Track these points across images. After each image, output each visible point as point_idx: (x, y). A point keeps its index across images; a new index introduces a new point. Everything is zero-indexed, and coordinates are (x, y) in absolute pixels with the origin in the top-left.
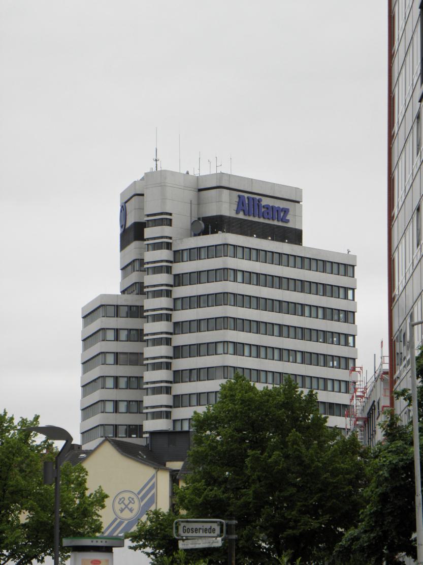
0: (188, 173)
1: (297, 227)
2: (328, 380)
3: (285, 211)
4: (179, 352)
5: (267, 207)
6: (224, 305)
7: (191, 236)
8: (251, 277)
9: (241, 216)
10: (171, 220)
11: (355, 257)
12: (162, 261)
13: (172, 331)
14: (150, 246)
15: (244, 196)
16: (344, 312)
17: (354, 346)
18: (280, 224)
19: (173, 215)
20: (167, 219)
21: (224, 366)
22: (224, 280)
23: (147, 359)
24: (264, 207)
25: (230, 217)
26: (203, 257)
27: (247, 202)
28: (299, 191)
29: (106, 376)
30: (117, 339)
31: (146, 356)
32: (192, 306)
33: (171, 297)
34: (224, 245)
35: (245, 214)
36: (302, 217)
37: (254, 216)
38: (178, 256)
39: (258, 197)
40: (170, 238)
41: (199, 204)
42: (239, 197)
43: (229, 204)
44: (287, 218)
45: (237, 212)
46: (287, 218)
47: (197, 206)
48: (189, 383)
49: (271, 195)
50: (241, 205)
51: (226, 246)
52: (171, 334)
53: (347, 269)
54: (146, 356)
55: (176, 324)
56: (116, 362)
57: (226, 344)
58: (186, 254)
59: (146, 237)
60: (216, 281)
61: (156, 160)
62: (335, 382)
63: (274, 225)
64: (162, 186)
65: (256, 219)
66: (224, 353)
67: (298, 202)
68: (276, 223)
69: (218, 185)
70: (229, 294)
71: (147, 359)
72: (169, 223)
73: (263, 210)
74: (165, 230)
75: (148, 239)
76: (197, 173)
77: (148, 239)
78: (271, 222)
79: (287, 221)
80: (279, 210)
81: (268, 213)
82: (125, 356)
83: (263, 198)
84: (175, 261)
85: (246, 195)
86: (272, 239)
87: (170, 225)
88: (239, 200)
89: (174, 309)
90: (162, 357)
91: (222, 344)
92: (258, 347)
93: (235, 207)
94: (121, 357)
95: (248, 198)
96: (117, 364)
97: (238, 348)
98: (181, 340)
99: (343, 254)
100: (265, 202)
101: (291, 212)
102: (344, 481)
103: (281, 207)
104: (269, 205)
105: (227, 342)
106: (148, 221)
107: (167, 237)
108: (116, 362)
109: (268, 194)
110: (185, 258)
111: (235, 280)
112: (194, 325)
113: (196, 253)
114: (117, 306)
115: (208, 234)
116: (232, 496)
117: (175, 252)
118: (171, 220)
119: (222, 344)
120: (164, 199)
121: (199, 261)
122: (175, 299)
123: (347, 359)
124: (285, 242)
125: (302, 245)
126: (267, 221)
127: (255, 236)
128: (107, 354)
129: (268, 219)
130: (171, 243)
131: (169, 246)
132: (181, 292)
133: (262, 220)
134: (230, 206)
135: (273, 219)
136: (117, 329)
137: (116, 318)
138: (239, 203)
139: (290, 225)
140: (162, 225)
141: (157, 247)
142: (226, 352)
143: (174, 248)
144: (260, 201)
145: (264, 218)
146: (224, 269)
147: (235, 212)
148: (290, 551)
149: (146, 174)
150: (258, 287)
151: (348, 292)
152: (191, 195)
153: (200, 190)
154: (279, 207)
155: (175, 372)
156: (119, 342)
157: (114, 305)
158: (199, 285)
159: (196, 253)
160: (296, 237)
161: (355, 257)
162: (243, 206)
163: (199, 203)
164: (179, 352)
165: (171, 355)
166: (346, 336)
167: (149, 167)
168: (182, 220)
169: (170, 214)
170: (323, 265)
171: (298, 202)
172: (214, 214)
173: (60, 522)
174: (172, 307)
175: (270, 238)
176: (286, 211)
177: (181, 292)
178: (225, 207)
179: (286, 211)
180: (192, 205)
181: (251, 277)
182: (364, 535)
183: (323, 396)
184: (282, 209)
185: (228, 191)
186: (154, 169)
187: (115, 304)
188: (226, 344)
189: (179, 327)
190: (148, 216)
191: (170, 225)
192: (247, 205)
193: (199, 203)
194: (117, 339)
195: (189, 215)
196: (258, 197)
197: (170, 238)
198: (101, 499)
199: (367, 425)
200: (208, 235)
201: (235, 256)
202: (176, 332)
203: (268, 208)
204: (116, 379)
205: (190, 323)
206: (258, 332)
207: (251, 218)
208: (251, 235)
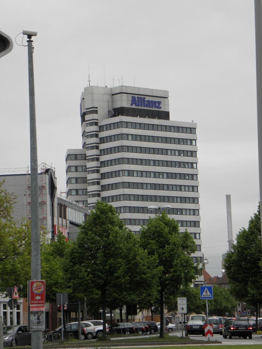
0: (106, 87)
1: (166, 110)
2: (182, 186)
3: (159, 103)
4: (103, 176)
5: (149, 101)
6: (122, 152)
7: (109, 118)
8: (136, 137)
9: (134, 106)
10: (97, 111)
11: (196, 123)
12: (93, 132)
13: (100, 166)
14: (88, 124)
15: (135, 97)
16: (190, 152)
17: (197, 168)
18: (157, 109)
19: (98, 108)
20: (95, 110)
21: (123, 182)
22: (122, 140)
23: (89, 180)
24: (147, 101)
25: (127, 108)
26: (112, 129)
27: (137, 99)
28: (167, 92)
29: (72, 189)
30: (76, 171)
31: (88, 179)
32: (108, 154)
33: (99, 149)
34: (121, 122)
35: (136, 106)
36: (169, 105)
37: (141, 106)
38: (101, 128)
39: (143, 97)
40: (97, 120)
41: (112, 102)
42: (132, 97)
43: (126, 101)
44: (160, 106)
45: (132, 105)
46: (160, 106)
47: (111, 103)
48: (108, 191)
49: (151, 95)
50: (134, 101)
51: (122, 122)
52: (99, 167)
53: (192, 130)
54: (88, 179)
55: (101, 162)
56: (77, 182)
57: (123, 171)
58: (105, 127)
59: (86, 120)
60: (118, 140)
61: (89, 81)
62: (186, 187)
63: (153, 110)
64: (92, 94)
65: (143, 108)
66: (123, 176)
67: (167, 98)
68: (154, 109)
69: (121, 92)
70: (124, 147)
71: (89, 180)
72: (96, 112)
73: (146, 103)
74: (94, 116)
75: (87, 121)
76: (112, 86)
77: (87, 121)
78: (151, 109)
79: (160, 108)
80: (155, 102)
81: (149, 104)
82: (81, 179)
83: (146, 97)
84: (100, 131)
85: (136, 96)
86: (149, 118)
87: (97, 113)
88: (132, 99)
89: (101, 155)
90: (95, 179)
91: (122, 171)
92: (142, 172)
93: (130, 102)
94: (79, 180)
95: (138, 97)
96: (77, 183)
97: (130, 173)
98: (104, 170)
99: (190, 123)
100: (147, 99)
101: (162, 103)
102: (82, 254)
103: (157, 101)
104: (149, 100)
105: (124, 170)
106: (86, 112)
107: (95, 120)
108: (77, 182)
109: (149, 95)
110: (105, 129)
111: (128, 139)
112: (109, 162)
113: (109, 127)
114: (76, 155)
115: (116, 116)
116: (82, 255)
117: (100, 127)
118: (97, 111)
119: (122, 171)
120: (93, 100)
121: (110, 131)
122: (101, 150)
123: (192, 175)
124: (156, 119)
125: (169, 120)
126: (149, 109)
127: (138, 116)
128: (72, 179)
129: (149, 107)
130: (98, 122)
131: (96, 124)
132: (103, 146)
133: (146, 108)
134: (127, 102)
135: (152, 107)
136: (76, 166)
137: (75, 161)
138: (132, 100)
139: (162, 110)
140: (93, 113)
141: (91, 124)
142: (123, 175)
143: (99, 125)
144: (144, 98)
145: (147, 107)
146: (121, 134)
147: (130, 105)
148: (130, 279)
149: (85, 88)
150: (141, 142)
151: (192, 142)
152: (108, 97)
153: (113, 95)
154: (155, 101)
155: (102, 186)
156: (77, 172)
157: (74, 154)
158: (111, 142)
159: (109, 127)
160: (166, 115)
161: (196, 123)
162: (135, 101)
163: (113, 102)
164: (103, 176)
165: (100, 178)
166: (192, 163)
167: (86, 85)
168: (103, 109)
169: (97, 108)
170: (178, 129)
171: (167, 98)
172: (119, 107)
173: (41, 268)
174: (99, 154)
175: (147, 117)
176: (159, 103)
177: (103, 146)
178: (125, 102)
179: (159, 103)
180: (109, 103)
181: (136, 137)
182: (148, 270)
183: (115, 204)
184: (157, 102)
185: (126, 94)
186: (88, 86)
187: (75, 154)
188: (123, 171)
189: (103, 164)
190: (87, 109)
191: (97, 113)
192: (137, 101)
193: (113, 102)
194: (76, 171)
195: (107, 107)
196: (143, 97)
197: (97, 120)
198: (179, 230)
199: (125, 222)
200: (116, 117)
201: (127, 127)
202: (102, 166)
203: (149, 102)
204: (77, 190)
205: (107, 162)
206: (141, 164)
207: (140, 107)
208: (137, 116)
